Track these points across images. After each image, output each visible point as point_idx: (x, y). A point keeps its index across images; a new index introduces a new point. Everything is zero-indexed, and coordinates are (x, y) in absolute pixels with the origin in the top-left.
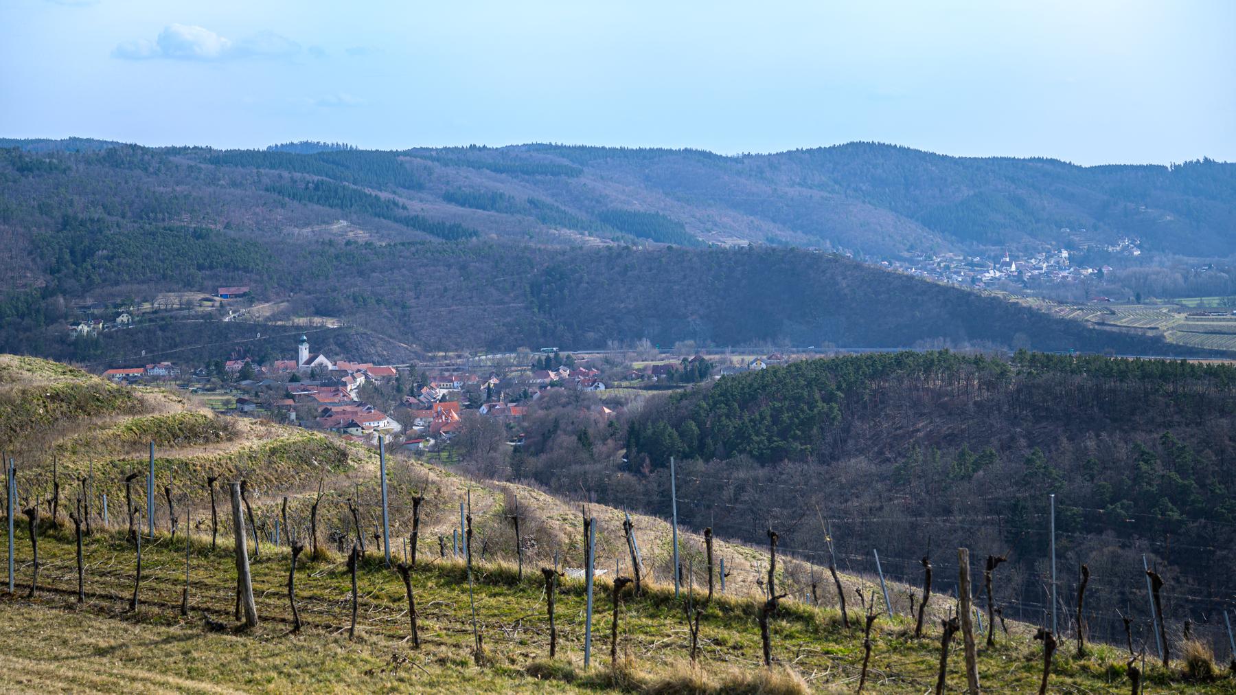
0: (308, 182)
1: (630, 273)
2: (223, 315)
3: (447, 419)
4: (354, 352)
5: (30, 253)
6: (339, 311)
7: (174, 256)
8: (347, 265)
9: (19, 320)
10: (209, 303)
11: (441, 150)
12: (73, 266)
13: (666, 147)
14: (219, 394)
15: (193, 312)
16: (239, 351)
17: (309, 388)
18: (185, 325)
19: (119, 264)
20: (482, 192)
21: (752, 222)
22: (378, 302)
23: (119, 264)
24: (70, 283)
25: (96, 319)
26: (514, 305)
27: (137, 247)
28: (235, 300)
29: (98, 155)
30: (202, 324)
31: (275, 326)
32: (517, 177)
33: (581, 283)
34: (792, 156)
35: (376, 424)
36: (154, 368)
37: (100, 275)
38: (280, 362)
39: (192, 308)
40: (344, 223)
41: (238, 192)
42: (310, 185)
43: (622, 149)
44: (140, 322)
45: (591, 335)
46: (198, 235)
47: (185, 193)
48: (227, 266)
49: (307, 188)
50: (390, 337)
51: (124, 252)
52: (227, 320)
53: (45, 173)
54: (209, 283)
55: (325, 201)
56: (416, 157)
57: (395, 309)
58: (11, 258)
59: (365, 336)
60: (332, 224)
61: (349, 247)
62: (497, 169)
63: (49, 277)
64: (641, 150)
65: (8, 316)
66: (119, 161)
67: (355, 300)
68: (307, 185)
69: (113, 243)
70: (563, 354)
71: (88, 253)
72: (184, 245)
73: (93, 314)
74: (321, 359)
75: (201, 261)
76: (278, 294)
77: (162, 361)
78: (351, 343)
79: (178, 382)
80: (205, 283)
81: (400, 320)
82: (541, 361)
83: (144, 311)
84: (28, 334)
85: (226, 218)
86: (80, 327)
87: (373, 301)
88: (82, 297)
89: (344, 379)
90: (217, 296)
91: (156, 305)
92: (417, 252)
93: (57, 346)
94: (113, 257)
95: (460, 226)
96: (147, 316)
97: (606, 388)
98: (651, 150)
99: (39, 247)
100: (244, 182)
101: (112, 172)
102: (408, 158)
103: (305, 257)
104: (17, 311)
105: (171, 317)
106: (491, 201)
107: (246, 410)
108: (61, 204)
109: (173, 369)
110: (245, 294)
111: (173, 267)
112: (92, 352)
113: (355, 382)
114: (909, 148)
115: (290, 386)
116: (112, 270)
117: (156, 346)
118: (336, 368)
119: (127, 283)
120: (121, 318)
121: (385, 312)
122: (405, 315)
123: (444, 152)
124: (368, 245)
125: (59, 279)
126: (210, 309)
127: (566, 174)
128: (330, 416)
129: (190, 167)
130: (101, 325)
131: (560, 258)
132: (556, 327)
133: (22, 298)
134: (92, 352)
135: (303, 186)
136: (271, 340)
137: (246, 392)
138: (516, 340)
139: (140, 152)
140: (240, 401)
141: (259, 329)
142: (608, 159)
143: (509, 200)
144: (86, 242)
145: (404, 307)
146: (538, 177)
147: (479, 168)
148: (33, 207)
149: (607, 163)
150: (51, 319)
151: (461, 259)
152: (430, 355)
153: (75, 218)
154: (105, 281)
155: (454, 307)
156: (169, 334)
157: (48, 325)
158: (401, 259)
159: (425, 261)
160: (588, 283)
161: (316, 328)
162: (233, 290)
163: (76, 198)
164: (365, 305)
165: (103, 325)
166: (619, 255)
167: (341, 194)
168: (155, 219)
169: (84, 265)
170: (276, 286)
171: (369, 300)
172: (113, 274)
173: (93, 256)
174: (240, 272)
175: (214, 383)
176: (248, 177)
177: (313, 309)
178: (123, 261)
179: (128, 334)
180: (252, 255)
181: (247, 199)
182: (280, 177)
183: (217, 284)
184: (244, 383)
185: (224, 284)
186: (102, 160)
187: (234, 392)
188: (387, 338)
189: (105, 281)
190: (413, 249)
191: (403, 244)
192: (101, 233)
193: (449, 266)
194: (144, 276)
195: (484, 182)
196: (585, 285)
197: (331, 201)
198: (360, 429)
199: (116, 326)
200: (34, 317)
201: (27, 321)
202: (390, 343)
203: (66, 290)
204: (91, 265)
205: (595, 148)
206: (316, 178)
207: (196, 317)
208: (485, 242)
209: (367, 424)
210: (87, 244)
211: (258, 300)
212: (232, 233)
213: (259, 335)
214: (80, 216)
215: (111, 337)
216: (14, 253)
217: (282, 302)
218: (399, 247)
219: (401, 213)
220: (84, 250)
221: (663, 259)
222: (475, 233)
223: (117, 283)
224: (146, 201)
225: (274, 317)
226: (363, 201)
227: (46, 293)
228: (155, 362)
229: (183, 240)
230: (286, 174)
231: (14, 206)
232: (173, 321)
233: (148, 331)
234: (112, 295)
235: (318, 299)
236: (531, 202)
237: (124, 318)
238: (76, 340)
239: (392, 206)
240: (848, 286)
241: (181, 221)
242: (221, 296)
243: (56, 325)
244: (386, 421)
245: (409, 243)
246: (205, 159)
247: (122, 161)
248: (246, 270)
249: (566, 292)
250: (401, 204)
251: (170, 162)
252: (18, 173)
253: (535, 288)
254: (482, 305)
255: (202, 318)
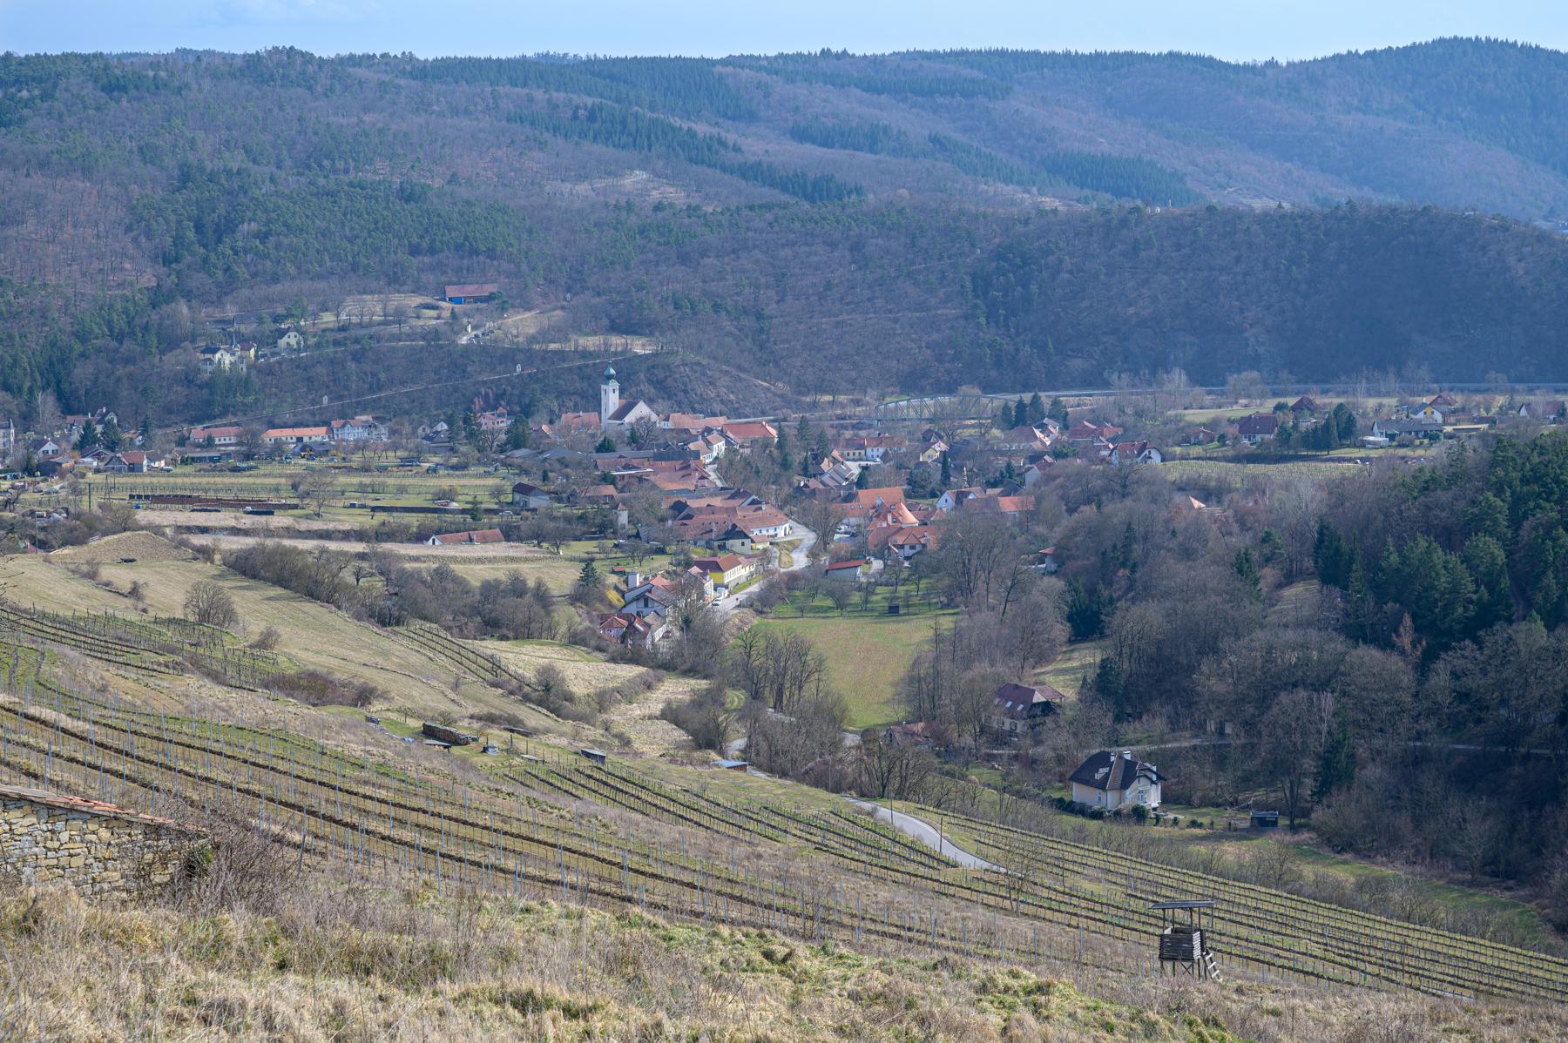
0: (577, 107)
1: (1143, 254)
2: (457, 333)
3: (896, 520)
4: (681, 395)
5: (129, 229)
6: (649, 325)
7: (369, 232)
8: (659, 244)
9: (114, 344)
10: (433, 313)
11: (776, 58)
12: (202, 250)
13: (1139, 49)
14: (476, 476)
15: (406, 329)
16: (487, 395)
17: (635, 462)
18: (393, 350)
19: (278, 246)
20: (854, 124)
21: (1289, 172)
22: (716, 308)
23: (278, 246)
24: (197, 280)
25: (245, 342)
26: (946, 311)
27: (307, 217)
28: (475, 306)
29: (231, 66)
30: (422, 348)
31: (546, 351)
32: (904, 100)
33: (1058, 272)
34: (1345, 63)
35: (772, 532)
36: (344, 426)
37: (246, 265)
38: (571, 415)
39: (405, 322)
40: (641, 175)
41: (465, 122)
42: (581, 112)
43: (1067, 55)
44: (318, 346)
45: (1077, 364)
46: (408, 195)
47: (380, 125)
48: (458, 247)
49: (575, 117)
50: (740, 368)
51: (285, 224)
52: (464, 340)
53: (147, 95)
54: (429, 278)
55: (607, 139)
56: (743, 67)
57: (744, 321)
58: (98, 236)
59: (698, 368)
60: (622, 176)
61: (660, 215)
62: (871, 88)
63: (162, 270)
64: (1098, 55)
65: (97, 338)
66: (266, 76)
67: (677, 306)
68: (575, 112)
69: (266, 211)
70: (1046, 398)
71: (226, 228)
72: (385, 213)
73: (237, 333)
74: (641, 410)
75: (415, 240)
76: (545, 296)
77: (356, 414)
78: (675, 380)
79: (398, 454)
80: (424, 278)
81: (754, 340)
82: (1010, 409)
83: (323, 326)
84: (131, 368)
85: (448, 168)
86: (218, 355)
87: (708, 306)
88: (219, 302)
89: (692, 446)
90: (444, 300)
91: (344, 317)
92: (776, 221)
93: (179, 388)
94: (267, 235)
95: (830, 179)
96: (330, 336)
97: (1163, 460)
98: (1115, 55)
99: (142, 219)
100: (472, 108)
101: (256, 93)
102: (730, 69)
103: (587, 231)
104: (111, 329)
105: (371, 337)
106: (872, 139)
107: (531, 506)
108: (175, 146)
109: (375, 427)
110: (490, 298)
111: (369, 249)
112: (239, 399)
113: (711, 450)
114: (1537, 47)
115: (604, 459)
116: (267, 256)
117: (346, 388)
118: (669, 425)
119: (293, 279)
120: (285, 339)
121: (728, 325)
122: (762, 330)
123: (781, 61)
124: (692, 210)
125: (179, 274)
126: (434, 322)
127: (986, 94)
128: (690, 517)
129: (382, 84)
130: (252, 351)
131: (1019, 228)
132: (1017, 350)
133: (119, 306)
134: (239, 399)
135: (569, 114)
136: (540, 376)
137: (525, 472)
138: (948, 372)
139: (299, 60)
140: (520, 489)
141: (520, 356)
142: (1045, 70)
143: (898, 139)
144: (222, 209)
145: (760, 316)
146: (940, 100)
147: (843, 86)
148: (131, 152)
149: (1043, 78)
150: (170, 342)
151: (852, 233)
152: (808, 399)
153: (202, 170)
154: (254, 275)
155: (844, 317)
156: (367, 367)
157: (162, 353)
158: (750, 234)
159: (792, 236)
160: (1071, 272)
161: (615, 354)
162: (471, 290)
163: (200, 135)
164: (695, 314)
165: (256, 352)
166: (1124, 222)
167: (633, 128)
168: (335, 171)
169: (220, 248)
170: (542, 282)
171: (701, 306)
172: (268, 263)
173: (234, 232)
174: (482, 258)
175: (465, 455)
176: (478, 100)
177: (605, 322)
178: (286, 241)
179: (298, 367)
180: (499, 229)
181: (481, 135)
182: (531, 99)
183: (444, 279)
184: (519, 453)
185: (455, 279)
186: (238, 74)
187: (503, 471)
188: (734, 372)
189: (254, 275)
190: (769, 216)
191: (751, 208)
192: (245, 193)
193: (833, 245)
194: (320, 266)
195: (853, 107)
196: (1067, 276)
197: (616, 139)
198: (747, 541)
199: (279, 354)
200: (139, 338)
201: (128, 345)
202: (740, 380)
203: (191, 291)
204: (232, 249)
205: (1022, 52)
206: (589, 101)
207: (411, 337)
208: (891, 203)
209: (756, 532)
210: (223, 212)
211: (513, 306)
212: (463, 192)
213: (519, 368)
214: (209, 166)
215: (271, 373)
216: (102, 228)
217: (554, 310)
218: (745, 212)
219: (731, 157)
220: (218, 225)
221: (1200, 229)
222: (859, 191)
223: (275, 279)
224: (315, 139)
225: (543, 336)
226: (670, 137)
227: (159, 297)
228: (346, 416)
229: (384, 204)
230: (539, 95)
231: (100, 150)
232: (374, 344)
233: (332, 362)
234: (269, 300)
235: (614, 304)
236: (934, 140)
237: (292, 339)
238: (211, 378)
239: (716, 146)
240: (1527, 273)
241: (375, 172)
242: (451, 299)
243: (175, 352)
244: (787, 525)
245: (761, 206)
246: (403, 72)
247: (272, 76)
248: (491, 254)
249: (1034, 288)
250: (731, 144)
251: (349, 76)
252: (103, 94)
253: (981, 283)
254: (890, 312)
255: (424, 338)
